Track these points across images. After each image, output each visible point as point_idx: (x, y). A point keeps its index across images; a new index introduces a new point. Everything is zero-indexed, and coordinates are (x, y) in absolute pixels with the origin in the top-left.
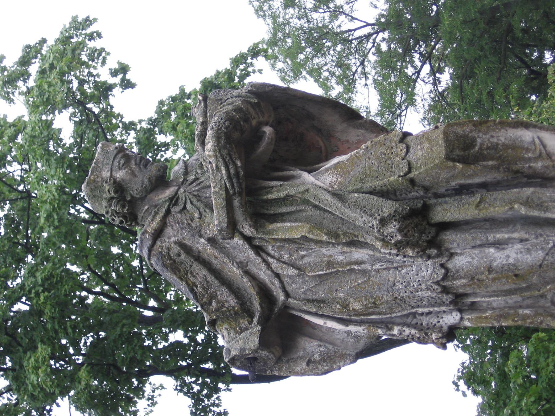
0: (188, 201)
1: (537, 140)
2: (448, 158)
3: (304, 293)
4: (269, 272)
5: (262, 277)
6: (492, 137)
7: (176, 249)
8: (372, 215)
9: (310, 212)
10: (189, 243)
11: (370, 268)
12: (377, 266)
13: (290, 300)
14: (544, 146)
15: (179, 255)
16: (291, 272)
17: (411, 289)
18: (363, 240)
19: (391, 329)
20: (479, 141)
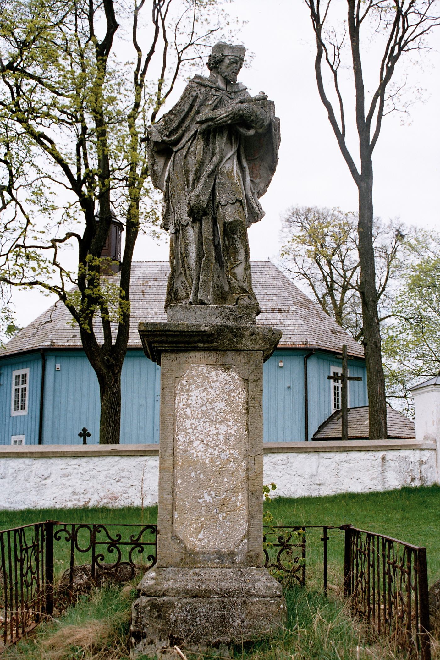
1: (240, 262)
14: (237, 266)
20: (236, 236)
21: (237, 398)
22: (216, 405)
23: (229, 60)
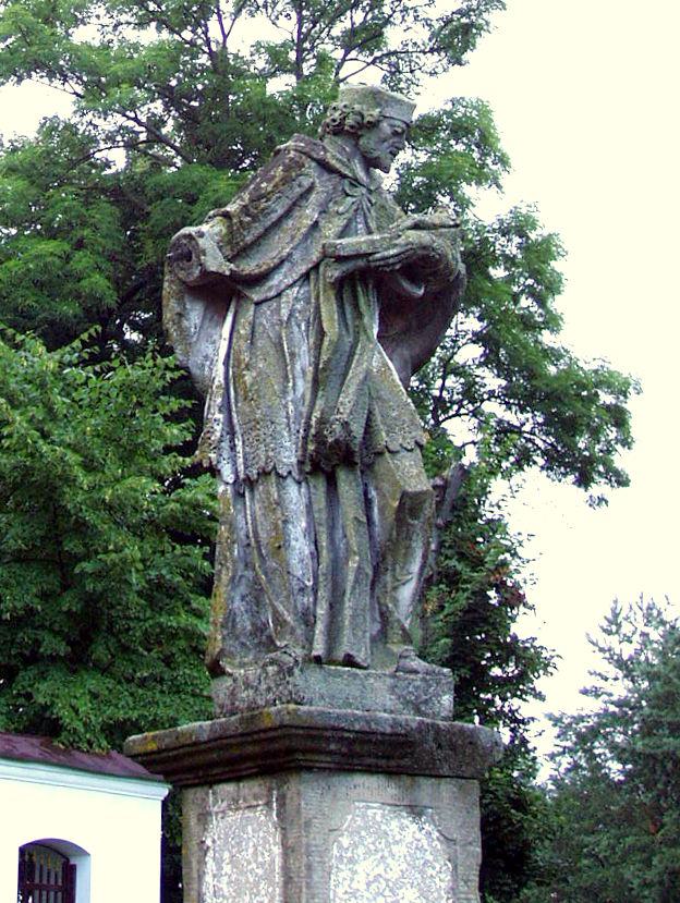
0: (354, 200)
2: (404, 494)
3: (261, 324)
4: (283, 286)
5: (276, 277)
6: (418, 535)
7: (306, 183)
8: (351, 413)
9: (349, 340)
10: (313, 197)
11: (289, 398)
12: (291, 407)
13: (252, 308)
14: (404, 584)
15: (300, 186)
16: (285, 313)
17: (268, 441)
18: (319, 396)
19: (220, 411)
20: (416, 522)
21: (437, 880)
22: (400, 892)
23: (392, 126)
